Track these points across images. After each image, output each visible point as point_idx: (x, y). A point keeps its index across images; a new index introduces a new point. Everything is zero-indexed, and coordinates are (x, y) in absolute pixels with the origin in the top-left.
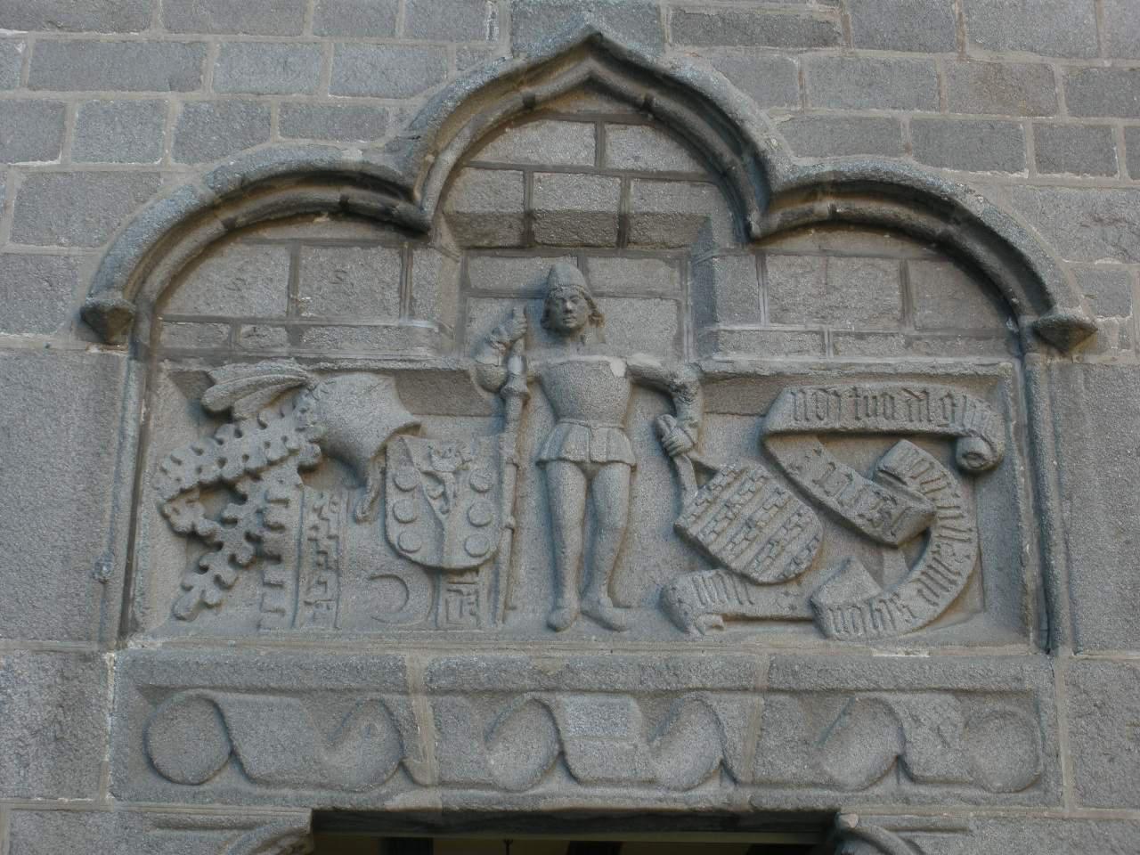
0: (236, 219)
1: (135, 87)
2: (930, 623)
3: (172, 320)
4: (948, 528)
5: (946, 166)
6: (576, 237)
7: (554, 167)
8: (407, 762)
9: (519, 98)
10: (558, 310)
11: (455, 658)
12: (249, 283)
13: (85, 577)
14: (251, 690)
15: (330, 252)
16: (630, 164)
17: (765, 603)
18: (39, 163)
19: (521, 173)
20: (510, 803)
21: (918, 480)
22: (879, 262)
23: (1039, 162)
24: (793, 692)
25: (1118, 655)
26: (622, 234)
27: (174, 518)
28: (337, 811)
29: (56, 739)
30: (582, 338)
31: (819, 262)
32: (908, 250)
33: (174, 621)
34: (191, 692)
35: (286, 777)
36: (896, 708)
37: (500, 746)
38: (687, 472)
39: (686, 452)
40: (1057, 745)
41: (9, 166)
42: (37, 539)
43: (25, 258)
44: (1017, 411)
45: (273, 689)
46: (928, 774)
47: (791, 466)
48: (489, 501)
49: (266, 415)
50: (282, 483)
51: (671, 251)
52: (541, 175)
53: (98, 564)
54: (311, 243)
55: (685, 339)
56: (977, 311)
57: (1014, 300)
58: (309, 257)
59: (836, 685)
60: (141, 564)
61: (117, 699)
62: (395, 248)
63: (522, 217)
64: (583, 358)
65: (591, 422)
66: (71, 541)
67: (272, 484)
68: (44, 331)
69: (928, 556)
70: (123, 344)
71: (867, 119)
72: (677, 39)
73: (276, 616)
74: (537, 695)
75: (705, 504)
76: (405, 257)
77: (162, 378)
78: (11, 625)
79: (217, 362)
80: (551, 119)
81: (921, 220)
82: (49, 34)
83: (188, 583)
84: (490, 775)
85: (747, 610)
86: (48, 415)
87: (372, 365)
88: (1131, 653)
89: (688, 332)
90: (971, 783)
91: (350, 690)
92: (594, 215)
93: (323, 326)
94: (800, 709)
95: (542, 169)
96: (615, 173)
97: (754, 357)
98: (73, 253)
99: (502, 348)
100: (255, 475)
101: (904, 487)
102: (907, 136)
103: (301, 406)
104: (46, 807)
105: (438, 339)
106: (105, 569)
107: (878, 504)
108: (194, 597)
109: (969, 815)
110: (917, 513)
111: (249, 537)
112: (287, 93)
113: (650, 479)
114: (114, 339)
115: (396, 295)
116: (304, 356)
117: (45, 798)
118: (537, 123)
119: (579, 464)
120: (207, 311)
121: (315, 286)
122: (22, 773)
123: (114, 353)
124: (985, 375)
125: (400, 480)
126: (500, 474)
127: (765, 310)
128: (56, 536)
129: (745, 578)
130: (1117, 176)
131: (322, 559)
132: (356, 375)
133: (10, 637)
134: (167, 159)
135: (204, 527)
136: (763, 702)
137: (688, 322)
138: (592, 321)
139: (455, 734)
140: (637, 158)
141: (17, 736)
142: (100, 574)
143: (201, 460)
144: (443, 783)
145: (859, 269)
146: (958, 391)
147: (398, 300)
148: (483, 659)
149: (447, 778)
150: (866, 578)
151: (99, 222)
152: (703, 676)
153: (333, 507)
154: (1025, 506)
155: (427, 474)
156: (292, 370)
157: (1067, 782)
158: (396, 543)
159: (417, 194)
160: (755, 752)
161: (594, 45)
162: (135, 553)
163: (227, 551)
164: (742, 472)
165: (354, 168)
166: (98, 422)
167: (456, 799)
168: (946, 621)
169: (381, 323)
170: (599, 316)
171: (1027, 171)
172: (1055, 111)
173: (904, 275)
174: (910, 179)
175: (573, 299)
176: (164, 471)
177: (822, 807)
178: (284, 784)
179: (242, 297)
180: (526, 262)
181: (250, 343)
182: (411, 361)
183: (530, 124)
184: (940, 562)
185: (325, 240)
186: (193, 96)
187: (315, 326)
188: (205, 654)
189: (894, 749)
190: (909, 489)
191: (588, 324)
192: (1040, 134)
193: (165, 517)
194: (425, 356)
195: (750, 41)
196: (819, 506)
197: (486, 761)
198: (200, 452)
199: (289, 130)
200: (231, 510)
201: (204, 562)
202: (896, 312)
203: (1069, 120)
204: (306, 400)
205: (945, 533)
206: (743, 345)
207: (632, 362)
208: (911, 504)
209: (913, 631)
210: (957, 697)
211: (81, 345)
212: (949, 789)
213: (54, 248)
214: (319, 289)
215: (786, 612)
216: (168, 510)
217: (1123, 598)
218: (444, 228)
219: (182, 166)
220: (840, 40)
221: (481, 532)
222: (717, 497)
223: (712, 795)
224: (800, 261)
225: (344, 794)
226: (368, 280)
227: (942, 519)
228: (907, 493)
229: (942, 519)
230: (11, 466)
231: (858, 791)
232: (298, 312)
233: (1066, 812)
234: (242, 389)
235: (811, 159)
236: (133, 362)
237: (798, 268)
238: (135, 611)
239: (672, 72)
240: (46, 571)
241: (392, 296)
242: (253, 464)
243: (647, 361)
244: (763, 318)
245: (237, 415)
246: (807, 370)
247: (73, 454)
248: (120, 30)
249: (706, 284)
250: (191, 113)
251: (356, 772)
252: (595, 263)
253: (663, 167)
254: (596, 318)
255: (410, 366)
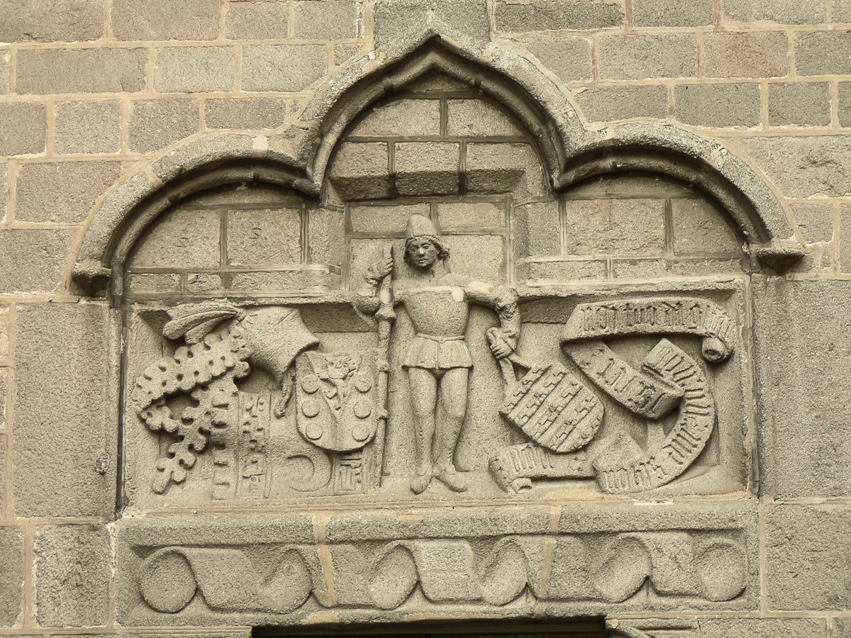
0: (179, 194)
1: (97, 89)
2: (677, 478)
3: (137, 273)
4: (694, 406)
5: (701, 124)
6: (428, 189)
7: (410, 137)
8: (315, 592)
9: (381, 89)
10: (415, 253)
11: (347, 517)
12: (191, 243)
13: (90, 471)
14: (207, 546)
15: (248, 214)
16: (466, 132)
17: (562, 466)
18: (30, 155)
19: (386, 144)
20: (385, 618)
21: (672, 372)
22: (649, 201)
23: (771, 116)
24: (576, 535)
25: (806, 501)
26: (461, 186)
27: (149, 420)
28: (268, 626)
29: (78, 585)
30: (433, 272)
31: (606, 203)
32: (674, 192)
33: (153, 495)
34: (168, 549)
35: (234, 605)
36: (647, 544)
37: (378, 578)
38: (508, 371)
39: (507, 357)
40: (758, 567)
41: (9, 159)
42: (54, 444)
43: (28, 232)
44: (745, 317)
45: (223, 544)
46: (667, 589)
47: (582, 362)
48: (368, 400)
49: (210, 339)
50: (223, 391)
51: (498, 195)
52: (401, 144)
53: (97, 461)
54: (236, 207)
55: (508, 266)
56: (720, 237)
57: (745, 232)
58: (235, 219)
59: (605, 528)
60: (128, 456)
61: (117, 556)
62: (296, 208)
63: (388, 178)
64: (433, 289)
65: (439, 338)
66: (78, 446)
67: (218, 393)
68: (46, 289)
69: (678, 427)
70: (104, 296)
71: (641, 87)
72: (500, 27)
73: (224, 487)
74: (401, 542)
75: (521, 395)
76: (303, 216)
77: (134, 317)
78: (40, 507)
79: (172, 304)
80: (408, 99)
81: (679, 170)
82: (28, 45)
83: (161, 466)
84: (371, 599)
85: (549, 472)
86: (54, 352)
87: (282, 301)
88: (814, 499)
89: (510, 261)
90: (697, 595)
91: (276, 544)
92: (439, 174)
93: (246, 273)
94: (581, 545)
95: (401, 139)
96: (455, 140)
97: (555, 282)
98: (62, 228)
99: (375, 282)
100: (204, 386)
101: (661, 378)
102: (672, 100)
103: (234, 333)
104: (74, 632)
105: (329, 279)
106: (103, 464)
107: (643, 391)
108: (165, 477)
109: (692, 617)
110: (670, 397)
111: (201, 431)
112: (209, 91)
113: (483, 375)
114: (98, 293)
115: (298, 245)
116: (234, 296)
117: (73, 626)
118: (396, 102)
119: (431, 370)
120: (163, 264)
121: (239, 242)
122: (56, 610)
123: (98, 303)
124: (723, 290)
125: (306, 386)
126: (376, 379)
127: (564, 243)
128: (68, 442)
129: (547, 450)
130: (830, 125)
131: (253, 445)
132: (272, 309)
133: (41, 516)
134: (124, 151)
135: (170, 425)
136: (555, 542)
137: (510, 252)
138: (439, 257)
139: (347, 572)
140: (470, 126)
141: (51, 585)
142: (100, 469)
143: (165, 376)
144: (339, 606)
145: (634, 208)
146: (703, 301)
147: (299, 249)
148: (365, 517)
149: (342, 603)
150: (633, 446)
151: (79, 202)
152: (515, 525)
153: (260, 407)
154: (747, 390)
155: (325, 380)
156: (226, 308)
157: (763, 593)
158: (304, 433)
159: (309, 170)
160: (549, 578)
161: (433, 43)
162: (123, 449)
163: (187, 442)
164: (547, 370)
165: (261, 156)
166: (91, 356)
167: (347, 616)
168: (687, 476)
169: (287, 268)
170: (445, 253)
171: (761, 124)
172: (786, 72)
173: (668, 210)
174: (669, 143)
175: (424, 246)
176: (140, 387)
177: (594, 615)
178: (234, 610)
179: (187, 252)
180: (393, 209)
181: (194, 288)
182: (310, 297)
183: (391, 103)
184: (686, 431)
185: (245, 204)
186: (138, 95)
187: (240, 273)
188: (175, 522)
189: (645, 572)
190: (664, 379)
191: (437, 260)
192: (775, 90)
193: (143, 421)
194: (320, 293)
195: (555, 24)
196: (602, 392)
197: (367, 589)
198: (163, 369)
199: (213, 123)
200: (189, 412)
201: (172, 450)
202: (660, 241)
203: (797, 78)
204: (236, 329)
205: (691, 409)
206: (548, 273)
207: (467, 290)
208: (666, 390)
209: (664, 484)
210: (690, 534)
211: (75, 298)
212: (682, 599)
213: (48, 224)
214: (242, 243)
215: (576, 473)
216: (144, 415)
217: (812, 458)
218: (331, 191)
219: (136, 155)
220: (625, 20)
221: (363, 422)
222: (529, 390)
223: (522, 607)
224: (591, 203)
225: (273, 615)
226: (277, 235)
227: (688, 399)
228: (663, 382)
229: (688, 399)
230: (32, 392)
231: (619, 602)
232: (228, 262)
233: (762, 615)
234: (191, 323)
235: (600, 123)
236: (112, 310)
237: (588, 212)
238: (126, 490)
239: (493, 64)
240: (61, 468)
241: (295, 246)
242: (202, 379)
243: (480, 288)
244: (562, 253)
245: (189, 342)
246: (593, 292)
247: (75, 381)
248: (81, 39)
249: (524, 223)
250: (139, 110)
251: (280, 596)
252: (443, 208)
253: (491, 134)
254: (442, 255)
255: (309, 301)
